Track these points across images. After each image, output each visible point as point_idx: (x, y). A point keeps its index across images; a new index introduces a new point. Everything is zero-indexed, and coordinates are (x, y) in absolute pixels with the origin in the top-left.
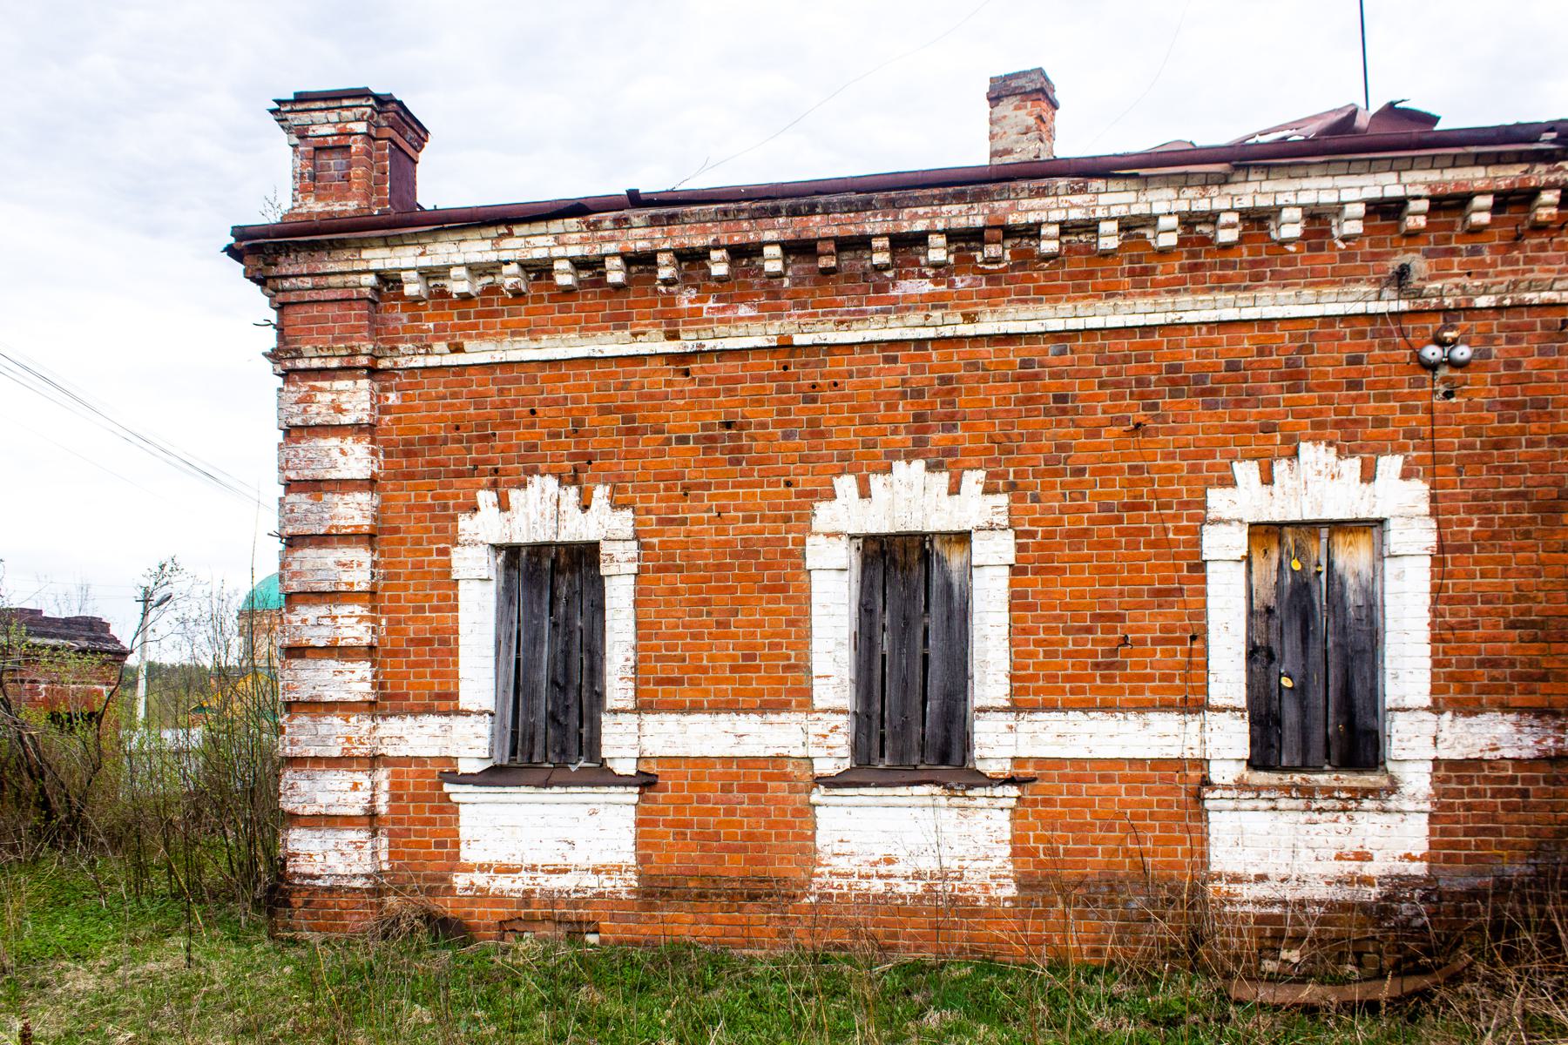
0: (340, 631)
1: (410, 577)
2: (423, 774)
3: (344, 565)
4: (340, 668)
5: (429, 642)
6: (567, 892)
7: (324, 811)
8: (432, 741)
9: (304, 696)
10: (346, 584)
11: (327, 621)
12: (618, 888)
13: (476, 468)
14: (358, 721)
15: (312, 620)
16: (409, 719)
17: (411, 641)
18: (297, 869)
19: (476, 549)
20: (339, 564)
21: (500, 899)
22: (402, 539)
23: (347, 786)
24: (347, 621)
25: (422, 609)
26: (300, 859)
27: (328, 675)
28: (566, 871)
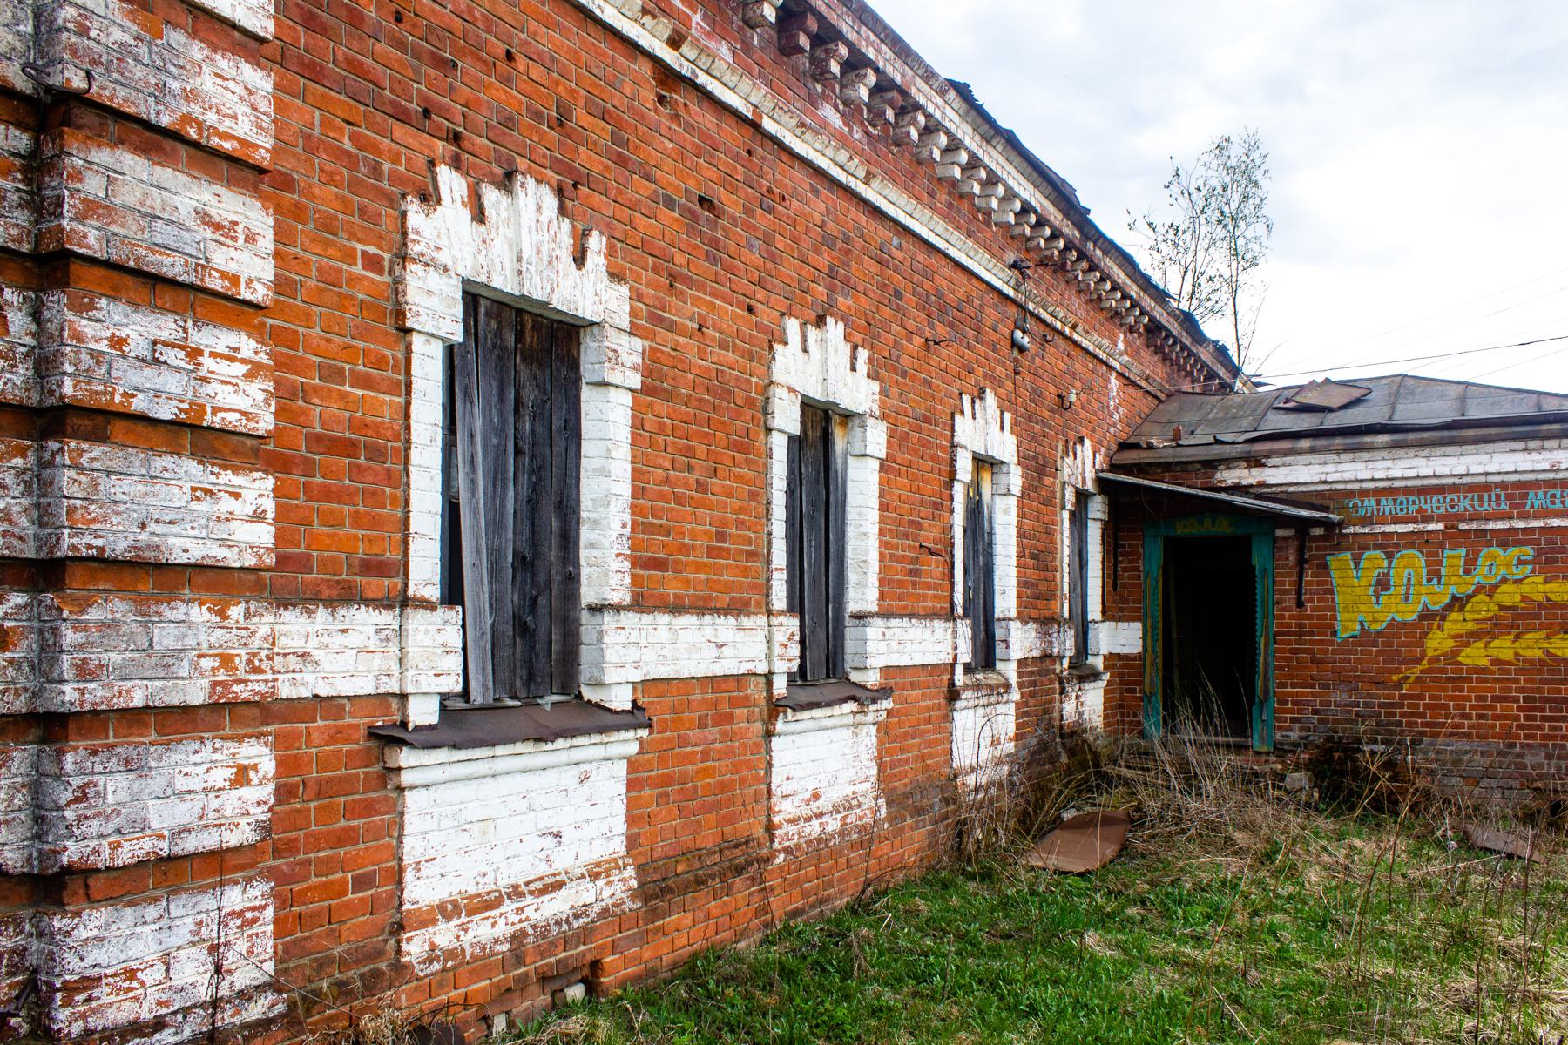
0: (209, 389)
1: (317, 298)
2: (337, 735)
3: (217, 227)
4: (208, 480)
5: (349, 448)
6: (567, 921)
7: (164, 847)
8: (365, 661)
9: (119, 546)
10: (224, 275)
11: (175, 357)
12: (619, 895)
13: (427, 113)
14: (248, 615)
15: (138, 346)
16: (322, 614)
17: (316, 440)
18: (95, 1022)
19: (444, 279)
20: (204, 218)
21: (481, 963)
22: (297, 205)
23: (221, 776)
24: (224, 368)
25: (337, 375)
26: (103, 994)
27: (177, 497)
28: (559, 885)
